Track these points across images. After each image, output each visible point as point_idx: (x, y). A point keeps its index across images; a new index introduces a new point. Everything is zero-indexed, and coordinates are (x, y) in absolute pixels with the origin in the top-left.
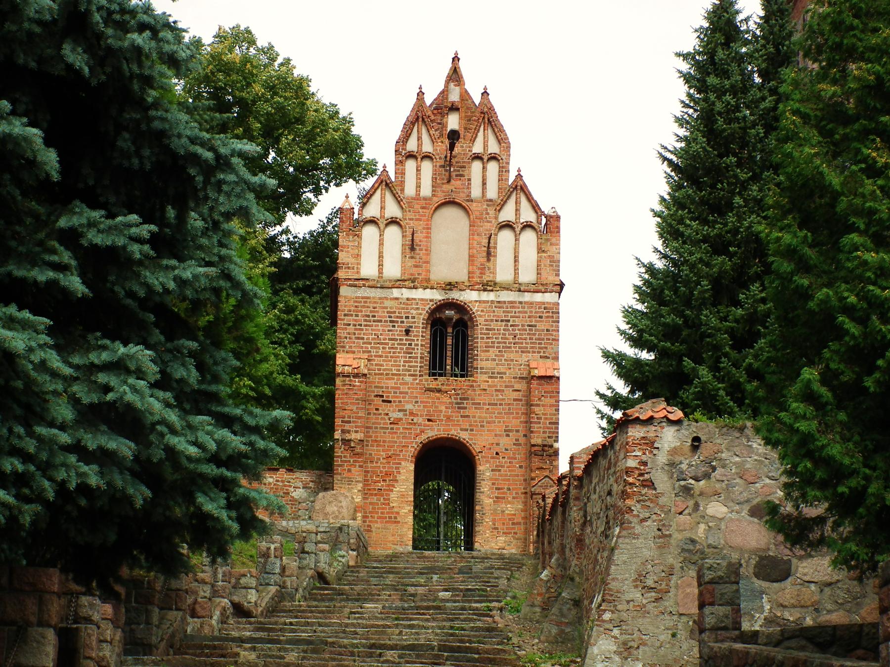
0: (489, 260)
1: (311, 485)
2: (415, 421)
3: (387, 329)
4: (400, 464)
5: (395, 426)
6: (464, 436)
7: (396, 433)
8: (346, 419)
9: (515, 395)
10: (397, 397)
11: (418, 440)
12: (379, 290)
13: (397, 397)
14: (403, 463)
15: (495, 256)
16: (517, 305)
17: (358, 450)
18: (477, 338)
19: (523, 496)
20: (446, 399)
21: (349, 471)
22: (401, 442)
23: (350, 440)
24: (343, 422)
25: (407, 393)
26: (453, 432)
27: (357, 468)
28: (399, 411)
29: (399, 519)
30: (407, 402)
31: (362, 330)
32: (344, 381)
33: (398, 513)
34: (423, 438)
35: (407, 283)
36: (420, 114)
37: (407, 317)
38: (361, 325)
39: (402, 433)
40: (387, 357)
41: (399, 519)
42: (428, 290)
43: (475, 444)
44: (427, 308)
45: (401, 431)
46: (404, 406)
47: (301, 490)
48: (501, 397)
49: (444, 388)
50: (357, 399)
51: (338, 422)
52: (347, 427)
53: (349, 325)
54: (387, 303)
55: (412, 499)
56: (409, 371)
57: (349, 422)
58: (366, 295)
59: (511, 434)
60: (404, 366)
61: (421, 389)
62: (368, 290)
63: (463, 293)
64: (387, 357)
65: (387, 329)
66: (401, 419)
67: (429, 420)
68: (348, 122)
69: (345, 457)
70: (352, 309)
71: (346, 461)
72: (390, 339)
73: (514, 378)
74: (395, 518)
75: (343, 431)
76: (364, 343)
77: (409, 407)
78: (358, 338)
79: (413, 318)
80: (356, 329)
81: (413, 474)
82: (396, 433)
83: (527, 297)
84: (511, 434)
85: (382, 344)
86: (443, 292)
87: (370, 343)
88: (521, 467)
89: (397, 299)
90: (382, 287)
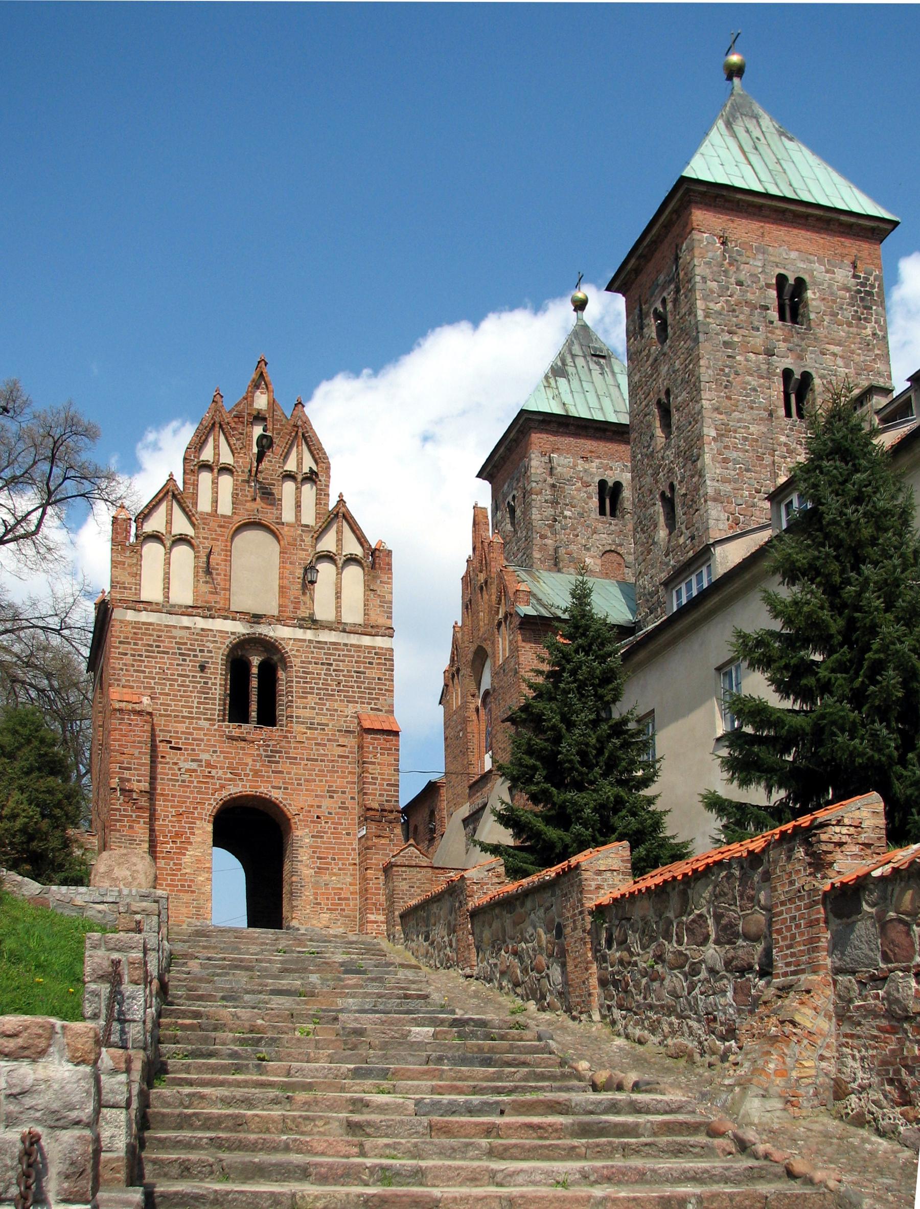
23: (131, 791)
25: (202, 740)
43: (290, 805)
53: (126, 654)
57: (129, 769)
70: (131, 635)
72: (179, 675)
76: (145, 677)
77: (205, 756)
79: (210, 652)
80: (135, 660)
86: (249, 625)
89: (188, 628)
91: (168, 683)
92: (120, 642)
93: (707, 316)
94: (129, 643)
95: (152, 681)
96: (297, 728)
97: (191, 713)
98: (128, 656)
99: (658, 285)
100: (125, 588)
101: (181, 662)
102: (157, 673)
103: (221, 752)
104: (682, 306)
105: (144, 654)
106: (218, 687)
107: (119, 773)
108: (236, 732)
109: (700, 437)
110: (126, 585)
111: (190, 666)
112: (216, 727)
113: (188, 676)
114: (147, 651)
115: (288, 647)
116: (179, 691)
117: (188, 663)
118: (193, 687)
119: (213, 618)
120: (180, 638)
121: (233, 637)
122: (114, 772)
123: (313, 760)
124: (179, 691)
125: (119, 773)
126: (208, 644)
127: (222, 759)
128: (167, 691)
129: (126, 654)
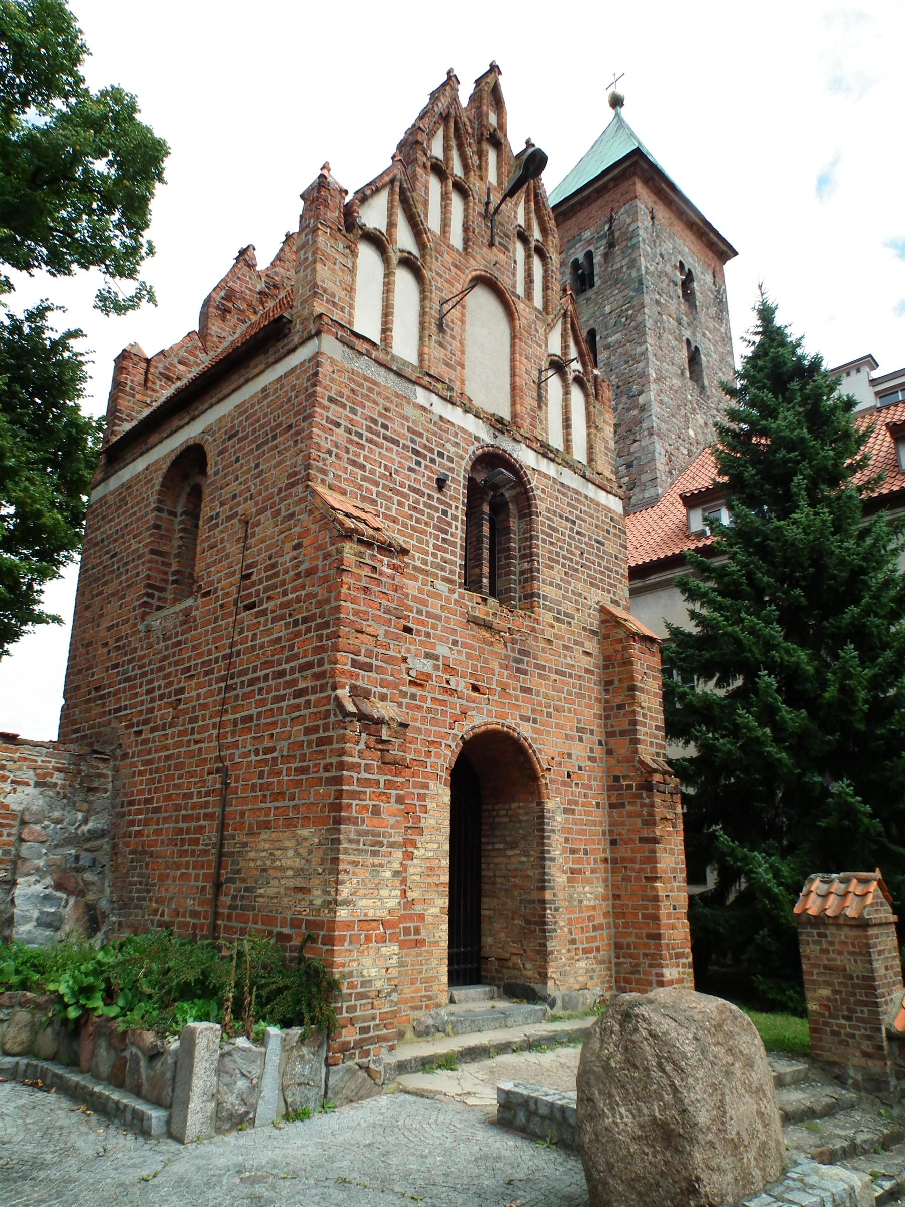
0: (540, 407)
1: (58, 778)
2: (453, 686)
3: (407, 464)
4: (426, 786)
5: (418, 691)
6: (525, 731)
7: (419, 708)
8: (361, 658)
9: (586, 662)
10: (423, 623)
11: (458, 731)
12: (392, 376)
13: (423, 623)
14: (432, 784)
15: (546, 405)
16: (582, 499)
17: (395, 753)
18: (538, 538)
19: (602, 866)
20: (499, 648)
21: (376, 811)
22: (429, 733)
23: (380, 721)
24: (355, 664)
25: (438, 618)
26: (509, 721)
27: (394, 806)
28: (428, 656)
29: (423, 935)
30: (440, 639)
31: (362, 447)
32: (361, 554)
33: (421, 917)
34: (465, 729)
35: (440, 386)
36: (452, 110)
37: (441, 455)
38: (360, 435)
39: (429, 710)
40: (405, 525)
41: (423, 935)
42: (470, 417)
43: (540, 750)
44: (471, 449)
45: (429, 704)
46: (434, 646)
47: (30, 790)
48: (569, 661)
49: (497, 622)
50: (387, 611)
51: (344, 662)
52: (364, 680)
53: (338, 425)
54: (409, 411)
55: (445, 878)
56: (443, 569)
57: (368, 668)
58: (368, 373)
59: (584, 736)
60: (434, 555)
61: (462, 615)
62: (374, 367)
63: (515, 444)
64: (405, 525)
65: (407, 464)
66: (429, 676)
67: (475, 688)
68: (149, 130)
69: (368, 769)
70: (346, 392)
71: (367, 782)
72: (411, 488)
73: (584, 629)
74: (417, 931)
75: (355, 692)
76: (364, 479)
77: (442, 650)
78: (354, 463)
79: (451, 459)
80: (351, 441)
81: (448, 809)
82: (419, 708)
83: (591, 491)
84: (584, 736)
85: (398, 493)
86: (492, 431)
87: (376, 484)
88: (598, 804)
89: (423, 409)
90: (398, 374)
91: (396, 498)
92: (331, 400)
93: (646, 272)
94: (344, 406)
95: (374, 489)
96: (546, 617)
97: (425, 562)
98: (341, 431)
99: (580, 240)
100: (334, 304)
101: (413, 466)
102: (382, 476)
103: (464, 645)
104: (617, 259)
105: (365, 434)
106: (459, 524)
107: (352, 675)
108: (480, 612)
109: (643, 375)
110: (336, 300)
111: (425, 478)
112: (456, 596)
113: (422, 494)
114: (369, 429)
115: (535, 482)
116: (411, 517)
117: (422, 469)
118: (429, 515)
119: (453, 404)
120: (414, 422)
121: (477, 444)
122: (343, 672)
123: (563, 674)
124: (411, 517)
125: (352, 675)
126: (448, 445)
127: (463, 658)
128: (393, 513)
129: (338, 425)
